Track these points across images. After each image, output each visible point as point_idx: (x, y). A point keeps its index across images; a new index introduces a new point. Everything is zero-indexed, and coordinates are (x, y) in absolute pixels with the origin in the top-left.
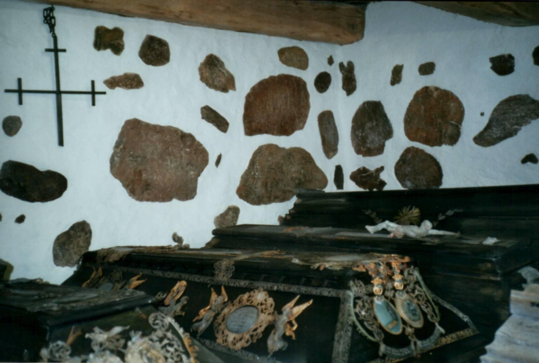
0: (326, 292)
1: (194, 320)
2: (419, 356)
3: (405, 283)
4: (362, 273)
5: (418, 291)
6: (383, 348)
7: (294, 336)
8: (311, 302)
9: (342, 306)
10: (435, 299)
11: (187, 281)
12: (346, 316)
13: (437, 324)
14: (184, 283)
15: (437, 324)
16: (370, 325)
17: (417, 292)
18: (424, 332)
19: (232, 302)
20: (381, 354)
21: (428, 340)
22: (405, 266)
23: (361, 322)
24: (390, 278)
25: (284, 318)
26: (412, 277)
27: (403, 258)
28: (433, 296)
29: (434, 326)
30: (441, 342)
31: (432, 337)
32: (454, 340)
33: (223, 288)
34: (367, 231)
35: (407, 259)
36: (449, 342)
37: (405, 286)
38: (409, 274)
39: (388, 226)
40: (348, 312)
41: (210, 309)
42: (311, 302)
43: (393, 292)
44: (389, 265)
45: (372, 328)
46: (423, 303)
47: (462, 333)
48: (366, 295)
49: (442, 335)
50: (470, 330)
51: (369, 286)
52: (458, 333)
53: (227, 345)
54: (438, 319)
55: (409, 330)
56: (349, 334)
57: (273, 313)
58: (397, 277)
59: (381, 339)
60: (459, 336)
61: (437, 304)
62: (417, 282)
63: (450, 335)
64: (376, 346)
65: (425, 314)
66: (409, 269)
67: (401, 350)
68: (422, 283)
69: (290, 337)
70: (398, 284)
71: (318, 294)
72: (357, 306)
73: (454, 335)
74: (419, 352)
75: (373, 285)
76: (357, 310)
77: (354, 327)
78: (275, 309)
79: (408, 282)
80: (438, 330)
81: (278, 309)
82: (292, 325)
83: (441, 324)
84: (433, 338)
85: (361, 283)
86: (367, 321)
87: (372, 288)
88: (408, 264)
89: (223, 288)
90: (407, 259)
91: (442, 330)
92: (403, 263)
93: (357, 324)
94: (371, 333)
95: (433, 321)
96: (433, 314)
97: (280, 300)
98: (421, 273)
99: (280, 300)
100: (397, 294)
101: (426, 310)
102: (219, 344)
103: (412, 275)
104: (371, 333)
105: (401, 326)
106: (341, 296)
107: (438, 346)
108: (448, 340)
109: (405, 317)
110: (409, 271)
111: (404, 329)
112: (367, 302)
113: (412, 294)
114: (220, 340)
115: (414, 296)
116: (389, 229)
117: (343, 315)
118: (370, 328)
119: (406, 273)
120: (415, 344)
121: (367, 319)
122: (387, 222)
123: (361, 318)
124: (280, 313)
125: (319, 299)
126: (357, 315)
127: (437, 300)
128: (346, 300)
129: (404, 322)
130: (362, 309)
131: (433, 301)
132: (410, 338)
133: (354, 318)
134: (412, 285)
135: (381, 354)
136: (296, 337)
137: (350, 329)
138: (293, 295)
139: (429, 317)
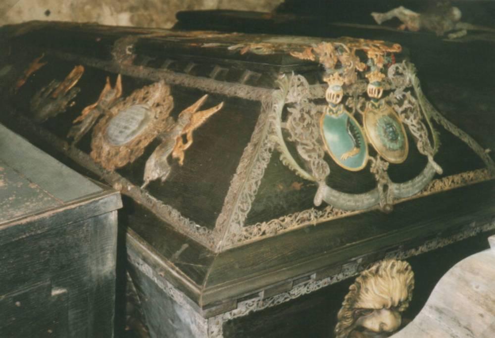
0: (242, 91)
1: (75, 121)
2: (388, 208)
3: (388, 87)
4: (307, 63)
5: (410, 102)
6: (323, 193)
7: (182, 159)
8: (221, 105)
9: (262, 116)
10: (436, 119)
11: (86, 67)
12: (265, 133)
13: (430, 159)
14: (81, 69)
15: (430, 159)
16: (308, 151)
17: (406, 105)
18: (399, 173)
19: (124, 100)
20: (318, 201)
21: (410, 183)
22: (391, 59)
23: (292, 147)
24: (361, 76)
25: (179, 131)
26: (400, 79)
27: (391, 46)
28: (434, 113)
29: (425, 160)
30: (433, 187)
31: (417, 179)
32: (457, 186)
33: (119, 78)
34: (373, 22)
35: (396, 48)
36: (447, 188)
37: (386, 93)
38: (397, 73)
39: (401, 13)
40: (270, 126)
41: (96, 107)
42: (221, 105)
43: (362, 100)
44: (362, 56)
45: (310, 156)
46: (414, 122)
47: (472, 174)
48: (310, 101)
49: (437, 176)
50: (486, 171)
51: (317, 86)
52: (465, 175)
53: (100, 162)
54: (436, 150)
55: (378, 166)
56: (264, 165)
57: (167, 119)
58: (374, 77)
59: (324, 177)
60: (467, 179)
61: (438, 127)
62: (410, 89)
63: (451, 177)
64: (311, 188)
65: (412, 140)
66: (397, 65)
67: (357, 197)
68: (418, 90)
69: (178, 159)
70: (372, 88)
71: (232, 94)
72: (290, 118)
73: (457, 178)
74: (390, 202)
75: (325, 85)
76: (288, 125)
77: (276, 154)
78: (171, 114)
79: (393, 87)
80: (432, 168)
81: (175, 114)
82: (185, 141)
83: (436, 159)
84: (419, 181)
85: (303, 79)
86: (302, 144)
87: (325, 91)
88: (398, 58)
89: (119, 78)
90: (396, 48)
91: (438, 169)
92: (389, 54)
93: (284, 148)
94: (302, 163)
95: (426, 153)
96: (428, 142)
97: (183, 98)
98: (419, 74)
99: (183, 98)
100: (369, 105)
101: (417, 135)
102: (91, 159)
103: (401, 74)
104: (302, 163)
105: (367, 157)
106: (263, 99)
107: (426, 193)
108: (445, 185)
109: (377, 144)
110: (397, 68)
111: (369, 163)
112: (308, 113)
113: (397, 108)
114: (94, 154)
115: (400, 110)
116: (401, 18)
117: (261, 131)
118: (305, 156)
119: (391, 70)
120: (385, 187)
121: (305, 142)
122: (402, 9)
123: (292, 139)
124: (176, 119)
125: (233, 102)
126: (286, 134)
127: (439, 121)
128: (269, 106)
129: (373, 152)
130: (298, 125)
131: (432, 120)
132: (377, 177)
133: (279, 138)
134: (398, 95)
135: (318, 201)
136: (184, 161)
137: (268, 156)
138: (198, 93)
139: (419, 145)
